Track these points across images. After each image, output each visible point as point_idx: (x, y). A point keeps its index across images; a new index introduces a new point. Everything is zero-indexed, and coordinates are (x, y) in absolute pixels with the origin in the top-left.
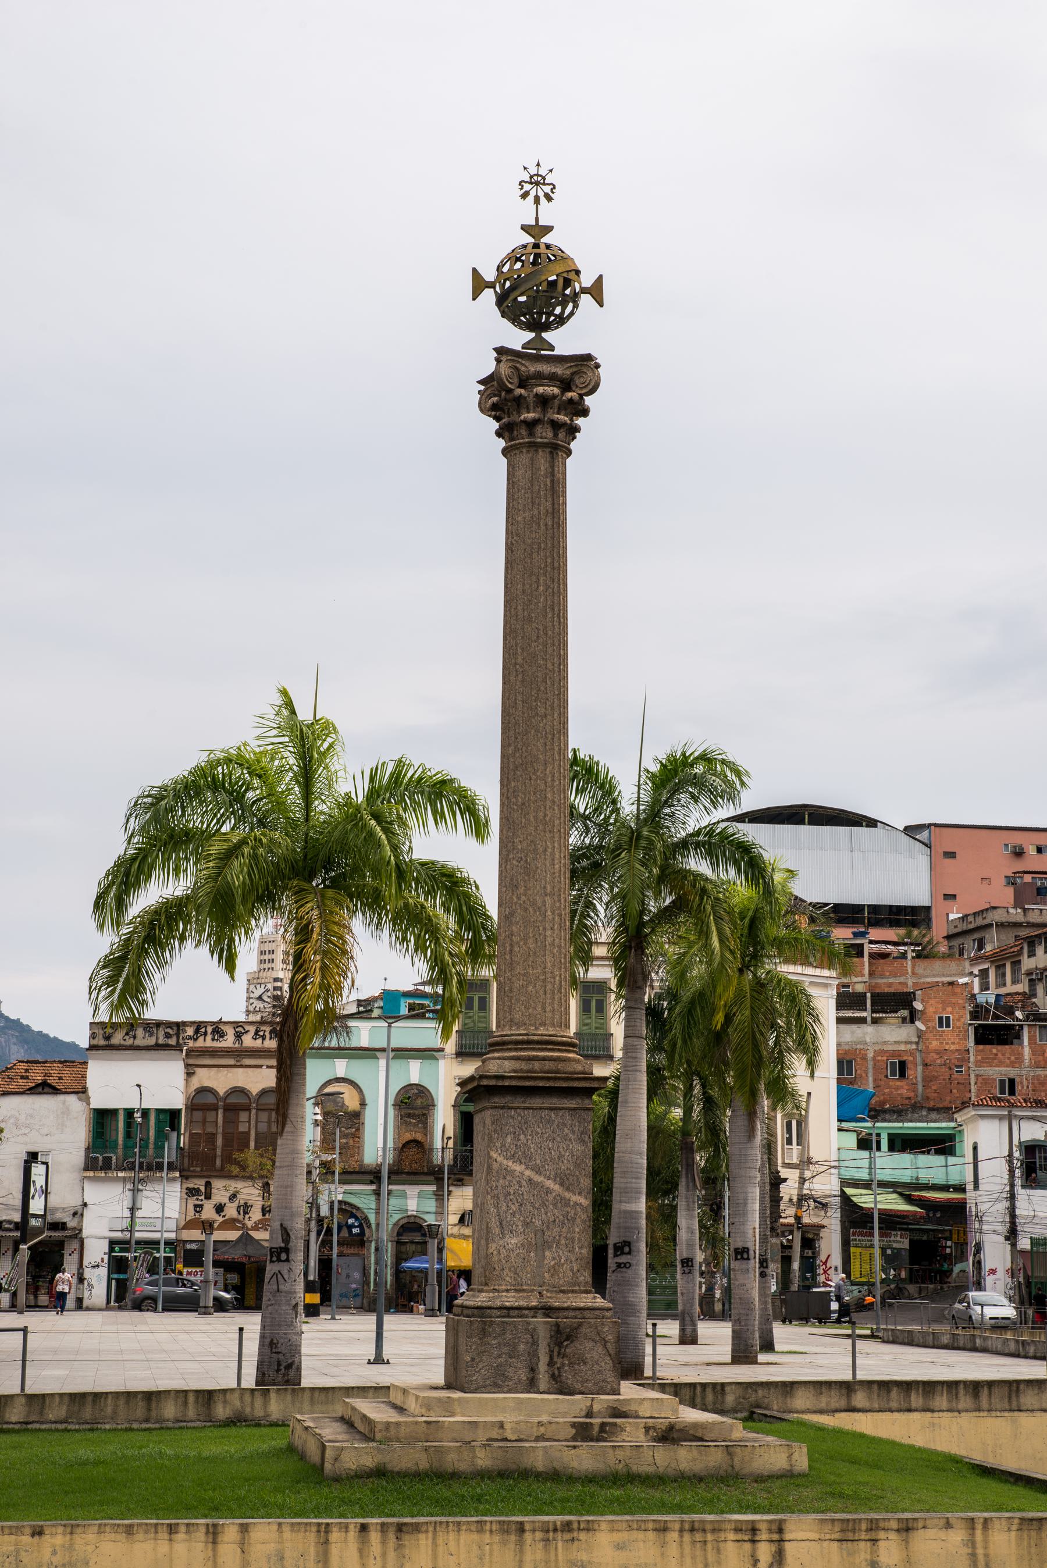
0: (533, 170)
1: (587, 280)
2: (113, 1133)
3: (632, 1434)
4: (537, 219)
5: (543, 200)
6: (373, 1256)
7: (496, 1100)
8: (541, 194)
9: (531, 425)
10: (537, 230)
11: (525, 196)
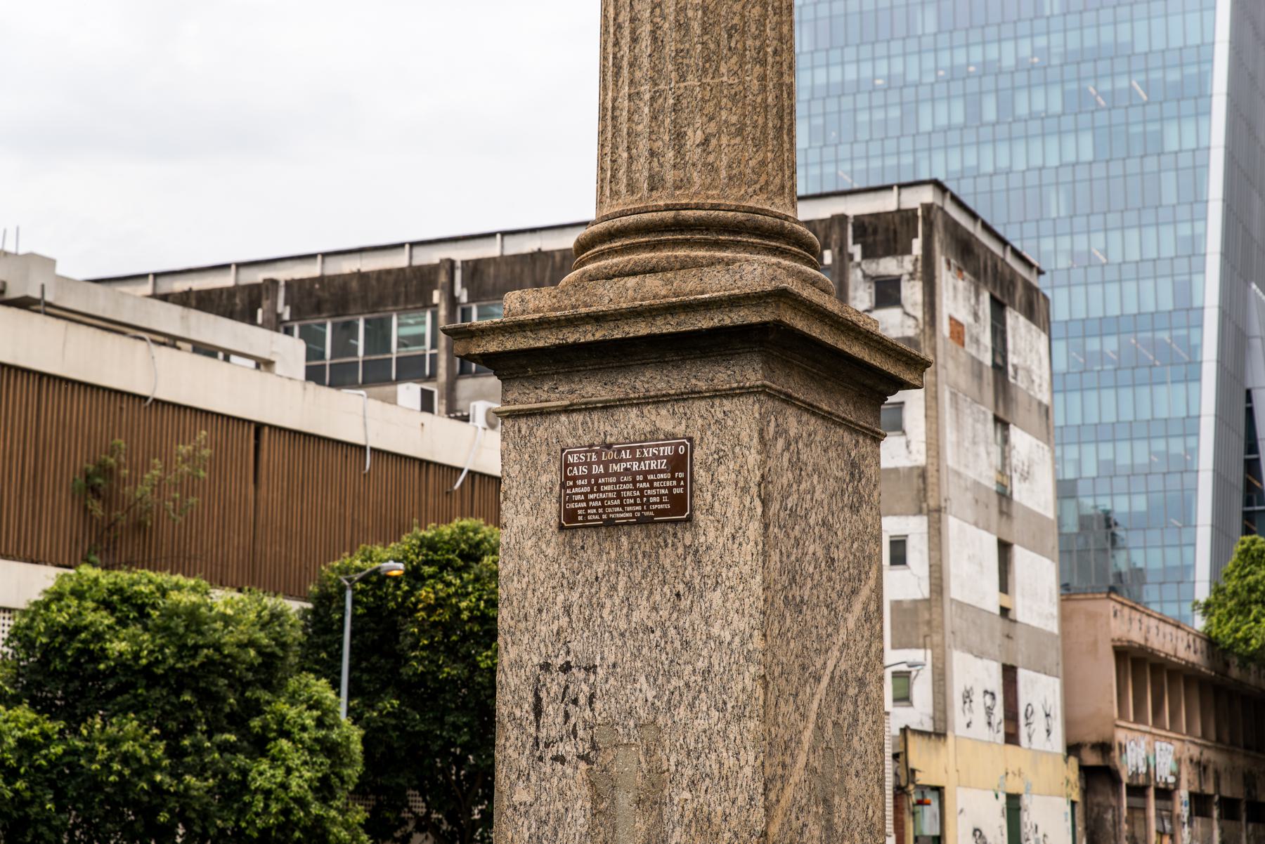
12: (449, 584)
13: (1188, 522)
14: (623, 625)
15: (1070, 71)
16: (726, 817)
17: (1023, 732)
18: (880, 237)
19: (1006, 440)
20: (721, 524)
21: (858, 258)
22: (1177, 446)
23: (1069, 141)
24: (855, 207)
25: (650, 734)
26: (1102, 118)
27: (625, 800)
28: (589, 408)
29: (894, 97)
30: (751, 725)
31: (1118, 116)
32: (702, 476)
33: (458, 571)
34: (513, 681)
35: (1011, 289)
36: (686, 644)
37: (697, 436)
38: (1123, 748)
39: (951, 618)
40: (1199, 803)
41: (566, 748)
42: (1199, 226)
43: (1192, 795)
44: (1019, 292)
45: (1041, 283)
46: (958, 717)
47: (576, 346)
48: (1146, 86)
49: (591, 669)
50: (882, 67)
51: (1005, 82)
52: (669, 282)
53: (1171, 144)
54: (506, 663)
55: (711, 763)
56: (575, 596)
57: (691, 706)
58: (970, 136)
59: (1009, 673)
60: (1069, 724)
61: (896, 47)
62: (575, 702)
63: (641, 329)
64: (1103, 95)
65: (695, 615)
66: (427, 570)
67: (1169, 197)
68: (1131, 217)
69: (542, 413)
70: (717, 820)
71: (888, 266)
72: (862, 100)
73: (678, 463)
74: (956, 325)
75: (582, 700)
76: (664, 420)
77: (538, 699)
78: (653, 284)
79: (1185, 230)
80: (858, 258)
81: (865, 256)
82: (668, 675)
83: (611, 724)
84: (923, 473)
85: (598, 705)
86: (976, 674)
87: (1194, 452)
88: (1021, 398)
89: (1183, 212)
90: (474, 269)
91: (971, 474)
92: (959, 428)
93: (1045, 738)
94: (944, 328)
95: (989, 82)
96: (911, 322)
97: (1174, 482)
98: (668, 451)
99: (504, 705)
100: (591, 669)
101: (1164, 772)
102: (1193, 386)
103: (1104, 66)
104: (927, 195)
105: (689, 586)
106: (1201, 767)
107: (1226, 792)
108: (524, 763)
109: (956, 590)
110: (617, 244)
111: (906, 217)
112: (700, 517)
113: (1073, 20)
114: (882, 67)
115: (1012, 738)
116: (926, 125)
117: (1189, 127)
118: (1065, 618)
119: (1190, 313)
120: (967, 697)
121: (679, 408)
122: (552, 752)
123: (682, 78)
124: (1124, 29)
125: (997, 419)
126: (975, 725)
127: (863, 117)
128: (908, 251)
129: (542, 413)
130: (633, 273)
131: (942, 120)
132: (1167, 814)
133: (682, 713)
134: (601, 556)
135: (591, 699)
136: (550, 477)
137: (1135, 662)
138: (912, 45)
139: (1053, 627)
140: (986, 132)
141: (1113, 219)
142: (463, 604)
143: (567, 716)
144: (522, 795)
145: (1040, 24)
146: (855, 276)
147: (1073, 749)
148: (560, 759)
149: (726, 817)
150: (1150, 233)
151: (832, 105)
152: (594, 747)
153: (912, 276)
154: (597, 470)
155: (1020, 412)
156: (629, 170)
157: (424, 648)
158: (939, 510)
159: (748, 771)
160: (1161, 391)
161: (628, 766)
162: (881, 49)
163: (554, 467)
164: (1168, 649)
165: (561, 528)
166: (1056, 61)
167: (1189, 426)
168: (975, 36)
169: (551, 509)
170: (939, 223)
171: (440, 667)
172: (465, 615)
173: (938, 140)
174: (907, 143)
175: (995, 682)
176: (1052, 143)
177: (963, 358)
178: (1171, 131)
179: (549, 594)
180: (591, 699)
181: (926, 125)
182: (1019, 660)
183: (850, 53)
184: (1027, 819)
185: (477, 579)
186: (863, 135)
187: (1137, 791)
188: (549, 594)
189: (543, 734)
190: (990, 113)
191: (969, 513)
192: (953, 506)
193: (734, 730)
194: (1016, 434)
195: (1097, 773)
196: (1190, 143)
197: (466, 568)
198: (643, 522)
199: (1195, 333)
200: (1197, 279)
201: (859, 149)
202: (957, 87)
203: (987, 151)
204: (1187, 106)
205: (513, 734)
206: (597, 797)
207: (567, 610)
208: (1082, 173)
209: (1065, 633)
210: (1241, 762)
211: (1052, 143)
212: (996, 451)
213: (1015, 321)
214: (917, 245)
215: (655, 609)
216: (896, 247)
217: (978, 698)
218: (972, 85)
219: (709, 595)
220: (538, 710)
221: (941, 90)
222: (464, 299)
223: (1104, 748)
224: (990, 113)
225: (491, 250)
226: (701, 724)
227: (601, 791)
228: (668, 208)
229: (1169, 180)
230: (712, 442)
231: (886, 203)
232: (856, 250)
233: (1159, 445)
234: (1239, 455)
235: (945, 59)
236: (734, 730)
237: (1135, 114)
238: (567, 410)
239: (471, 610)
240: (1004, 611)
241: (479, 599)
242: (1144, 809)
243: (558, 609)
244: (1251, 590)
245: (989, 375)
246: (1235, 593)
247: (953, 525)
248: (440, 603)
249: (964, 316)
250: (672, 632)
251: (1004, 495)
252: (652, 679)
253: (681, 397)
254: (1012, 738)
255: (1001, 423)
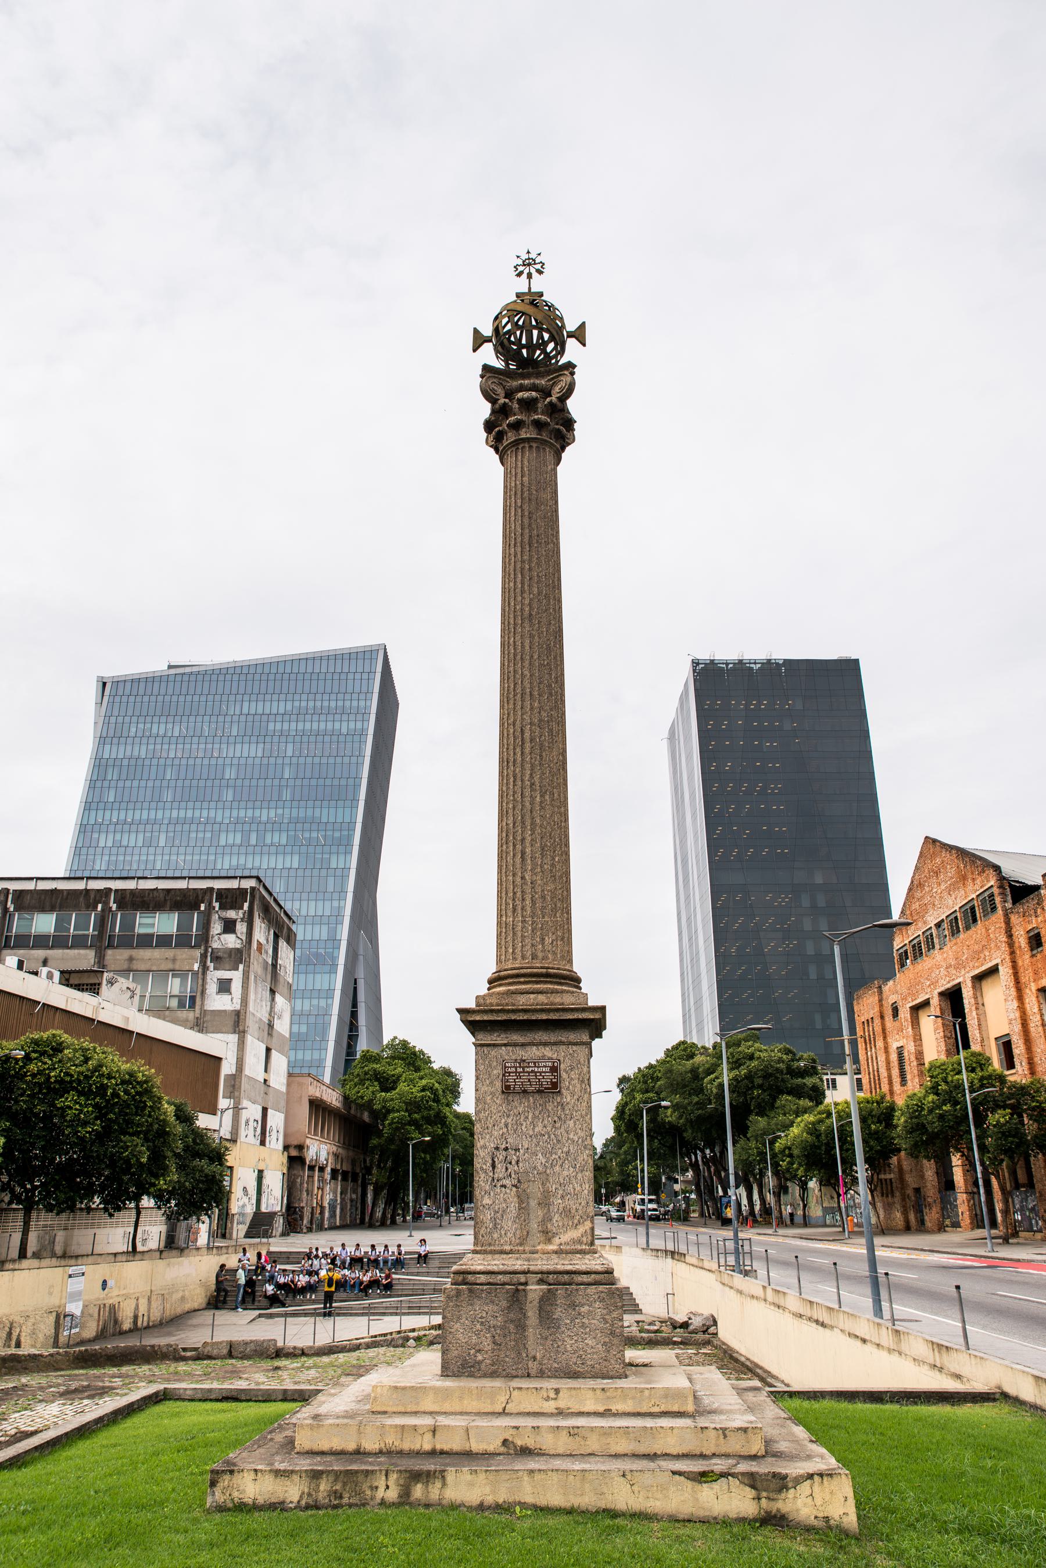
0: (525, 256)
1: (571, 326)
2: (188, 1392)
3: (354, 1196)
4: (530, 288)
5: (535, 274)
6: (979, 1175)
7: (515, 1037)
8: (533, 271)
9: (517, 426)
10: (533, 300)
11: (519, 275)
12: (45, 1063)
13: (324, 1039)
14: (531, 1133)
15: (292, 826)
16: (577, 1210)
17: (268, 1139)
18: (229, 900)
19: (273, 999)
20: (573, 1094)
21: (217, 909)
22: (323, 1003)
23: (288, 858)
24: (218, 885)
25: (543, 1177)
26: (304, 849)
27: (533, 1203)
28: (515, 1045)
29: (209, 827)
30: (587, 1174)
31: (311, 849)
32: (564, 1075)
33: (50, 1057)
34: (482, 1154)
35: (282, 929)
36: (558, 1141)
37: (562, 1059)
38: (308, 1147)
39: (245, 1085)
40: (334, 1172)
41: (507, 1182)
42: (342, 903)
43: (332, 1169)
44: (285, 930)
45: (294, 927)
46: (242, 1133)
47: (515, 1021)
48: (325, 837)
49: (517, 1150)
50: (205, 813)
51: (262, 827)
52: (548, 998)
53: (333, 865)
54: (479, 1145)
55: (570, 1188)
56: (509, 1120)
57: (561, 1166)
58: (243, 850)
59: (265, 1110)
60: (285, 1136)
61: (213, 805)
62: (510, 1163)
63: (544, 1017)
64: (305, 839)
65: (562, 1130)
66: (34, 1055)
67: (330, 889)
68: (313, 896)
69: (494, 1045)
70: (573, 1211)
71: (231, 914)
72: (194, 827)
73: (554, 1069)
74: (259, 944)
75: (513, 1162)
76: (548, 1052)
77: (494, 1162)
78: (541, 998)
79: (335, 904)
80: (217, 909)
81: (220, 908)
82: (551, 1153)
83: (527, 1173)
84: (237, 1013)
85: (521, 1165)
86: (252, 1111)
87: (329, 1006)
88: (281, 980)
89: (336, 896)
90: (19, 895)
91: (259, 1015)
92: (256, 993)
93: (275, 1142)
94: (255, 945)
95: (254, 827)
96: (239, 941)
97: (320, 1020)
98: (550, 1064)
99: (478, 1163)
100: (517, 1150)
101: (322, 1159)
102: (333, 975)
103: (307, 826)
104: (252, 883)
105: (559, 1118)
106: (336, 1156)
107: (345, 1168)
108: (487, 1188)
109: (247, 1071)
110: (522, 980)
111: (242, 892)
112: (564, 1091)
113: (295, 804)
114: (205, 813)
115: (263, 1143)
116: (223, 842)
117: (342, 857)
118: (289, 1085)
119: (335, 941)
120: (247, 1122)
121: (554, 1048)
122: (500, 1183)
123: (543, 917)
124: (317, 811)
125: (271, 990)
126: (248, 1136)
127: (193, 835)
128: (242, 908)
129: (494, 1045)
130: (533, 993)
131: (230, 841)
132: (322, 1179)
133: (557, 1169)
134: (520, 1105)
135: (517, 1162)
136: (497, 1071)
137: (317, 1106)
138: (220, 805)
139: (284, 1089)
140: (250, 849)
141: (305, 896)
142: (52, 1074)
143: (507, 1169)
144: (487, 1201)
145: (280, 804)
146: (215, 917)
147: (286, 1148)
148: (504, 1186)
149: (577, 1210)
150: (320, 904)
151: (179, 828)
152: (519, 1181)
153: (242, 920)
154: (519, 1070)
155: (281, 987)
156: (522, 951)
157: (28, 1095)
158: (244, 1032)
159: (586, 1192)
160: (318, 977)
161: (535, 1189)
162: (205, 805)
163: (500, 1068)
164: (329, 1100)
165: (503, 1092)
166: (286, 821)
167: (329, 993)
168: (250, 804)
169: (498, 1084)
170: (257, 896)
171: (35, 1106)
172: (53, 1080)
173: (228, 850)
174: (212, 850)
175: (259, 1117)
176: (280, 858)
177: (261, 960)
178: (334, 858)
179: (498, 1118)
180: (517, 1162)
181: (223, 842)
182: (269, 1105)
183: (190, 805)
184: (265, 1182)
185: (60, 1061)
186: (192, 844)
187: (312, 1168)
188: (498, 1118)
189: (496, 1176)
190: (253, 841)
191: (256, 1034)
192: (250, 1030)
193: (580, 1175)
194: (278, 998)
195: (296, 1160)
196: (341, 866)
197: (53, 1056)
198: (539, 1092)
199: (336, 951)
200: (339, 926)
201: (190, 850)
202: (239, 827)
203: (250, 858)
204: (342, 849)
205: (483, 1176)
206: (521, 1202)
207: (506, 1126)
208: (292, 873)
209: (288, 1092)
210: (351, 1154)
211: (280, 858)
212: (269, 1004)
213: (283, 944)
214: (246, 906)
215: (545, 1127)
216: (236, 906)
217: (251, 1123)
218: (247, 827)
219: (568, 1122)
220: (494, 1166)
221: (231, 827)
222: (12, 909)
223: (300, 1147)
224: (253, 841)
225: (30, 886)
226: (565, 1173)
227: (523, 1199)
228: (542, 968)
229: (331, 880)
230: (568, 1062)
231: (234, 884)
232: (217, 905)
233: (315, 1002)
234: (349, 1008)
235: (235, 813)
236: (580, 1175)
237: (319, 849)
238: (505, 1045)
239: (55, 1076)
240: (265, 1081)
241: (61, 1071)
242: (313, 1177)
243: (502, 1125)
244: (366, 1073)
245: (270, 968)
246: (358, 1075)
247: (249, 1039)
248: (40, 1072)
249: (263, 941)
250: (552, 1136)
251: (271, 1026)
252: (544, 1155)
253: (555, 1044)
254: (263, 1143)
255: (273, 992)
